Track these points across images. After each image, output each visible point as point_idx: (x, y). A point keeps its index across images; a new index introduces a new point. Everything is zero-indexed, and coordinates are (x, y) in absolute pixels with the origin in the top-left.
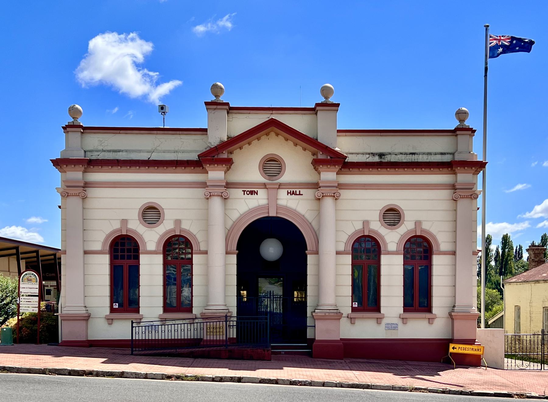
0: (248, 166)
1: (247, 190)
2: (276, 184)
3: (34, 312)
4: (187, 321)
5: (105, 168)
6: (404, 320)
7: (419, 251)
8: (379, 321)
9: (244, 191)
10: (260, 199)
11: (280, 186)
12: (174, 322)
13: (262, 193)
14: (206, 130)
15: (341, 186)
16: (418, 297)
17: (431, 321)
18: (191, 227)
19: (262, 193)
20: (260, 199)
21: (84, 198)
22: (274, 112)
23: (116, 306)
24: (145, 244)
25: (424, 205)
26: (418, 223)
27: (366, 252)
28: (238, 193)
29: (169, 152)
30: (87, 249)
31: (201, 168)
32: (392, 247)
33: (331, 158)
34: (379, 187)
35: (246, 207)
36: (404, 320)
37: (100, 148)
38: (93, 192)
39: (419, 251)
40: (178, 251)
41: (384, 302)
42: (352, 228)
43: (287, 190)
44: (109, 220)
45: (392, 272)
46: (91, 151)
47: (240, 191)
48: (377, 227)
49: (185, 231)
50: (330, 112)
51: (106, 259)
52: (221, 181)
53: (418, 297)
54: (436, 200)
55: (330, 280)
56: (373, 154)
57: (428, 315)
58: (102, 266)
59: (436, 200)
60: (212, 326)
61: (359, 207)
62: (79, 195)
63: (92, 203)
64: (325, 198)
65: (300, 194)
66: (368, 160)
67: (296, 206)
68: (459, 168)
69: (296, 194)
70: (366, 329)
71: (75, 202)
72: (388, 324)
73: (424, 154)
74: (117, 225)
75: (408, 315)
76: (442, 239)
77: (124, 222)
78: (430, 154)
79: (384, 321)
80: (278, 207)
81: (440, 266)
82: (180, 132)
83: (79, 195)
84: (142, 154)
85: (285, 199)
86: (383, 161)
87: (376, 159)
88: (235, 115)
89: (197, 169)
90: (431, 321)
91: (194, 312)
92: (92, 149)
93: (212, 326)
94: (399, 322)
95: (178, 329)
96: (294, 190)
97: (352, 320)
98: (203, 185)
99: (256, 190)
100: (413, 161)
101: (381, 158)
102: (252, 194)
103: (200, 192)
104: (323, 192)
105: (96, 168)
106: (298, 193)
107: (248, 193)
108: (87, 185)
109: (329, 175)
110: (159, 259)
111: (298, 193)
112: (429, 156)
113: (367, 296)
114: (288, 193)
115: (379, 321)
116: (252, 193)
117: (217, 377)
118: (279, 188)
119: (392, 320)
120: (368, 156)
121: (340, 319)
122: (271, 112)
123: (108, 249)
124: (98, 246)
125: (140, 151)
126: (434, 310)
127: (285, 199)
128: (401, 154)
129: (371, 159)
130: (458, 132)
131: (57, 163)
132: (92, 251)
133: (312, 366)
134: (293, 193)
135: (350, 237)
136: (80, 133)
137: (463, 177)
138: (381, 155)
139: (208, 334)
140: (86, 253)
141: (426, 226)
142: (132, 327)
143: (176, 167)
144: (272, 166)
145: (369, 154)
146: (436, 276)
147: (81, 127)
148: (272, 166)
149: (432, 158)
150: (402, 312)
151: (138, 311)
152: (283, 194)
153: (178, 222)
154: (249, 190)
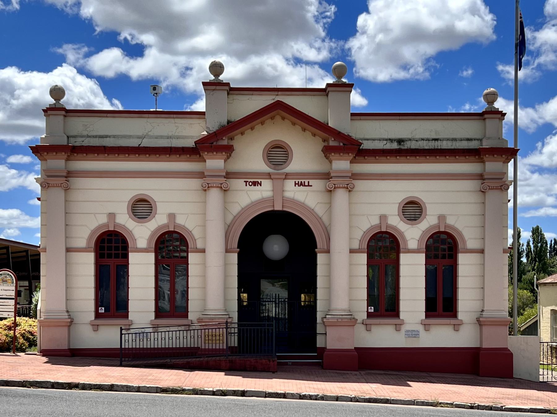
0: (251, 154)
1: (249, 180)
6: (427, 327)
7: (443, 250)
8: (398, 327)
9: (246, 182)
10: (265, 190)
11: (287, 176)
13: (267, 185)
15: (355, 176)
16: (441, 301)
18: (187, 222)
19: (267, 185)
20: (265, 190)
21: (67, 189)
22: (280, 93)
23: (102, 310)
24: (405, 241)
25: (448, 200)
28: (239, 183)
29: (162, 137)
31: (198, 156)
32: (142, 243)
35: (249, 199)
36: (427, 327)
37: (85, 133)
38: (79, 183)
39: (443, 250)
40: (172, 249)
42: (367, 223)
43: (294, 180)
44: (95, 214)
45: (413, 273)
47: (292, 182)
48: (396, 222)
51: (90, 258)
52: (220, 170)
53: (441, 301)
55: (342, 282)
56: (391, 140)
57: (453, 321)
58: (86, 265)
61: (379, 200)
65: (309, 185)
67: (306, 199)
70: (384, 337)
71: (58, 194)
76: (469, 237)
77: (383, 218)
79: (404, 328)
80: (284, 200)
81: (466, 265)
82: (175, 116)
83: (61, 186)
84: (131, 140)
85: (292, 190)
86: (402, 147)
87: (395, 146)
88: (235, 97)
90: (456, 327)
92: (76, 134)
94: (421, 328)
96: (302, 178)
98: (201, 175)
99: (259, 181)
101: (400, 144)
102: (255, 185)
103: (195, 183)
104: (335, 182)
106: (306, 184)
107: (251, 184)
108: (70, 174)
109: (342, 164)
110: (151, 257)
111: (306, 184)
112: (454, 143)
113: (384, 301)
114: (295, 184)
116: (255, 184)
118: (285, 179)
119: (413, 327)
120: (385, 142)
122: (276, 93)
124: (82, 243)
125: (130, 137)
126: (460, 316)
127: (292, 190)
128: (423, 139)
130: (486, 116)
134: (302, 184)
138: (400, 141)
140: (68, 250)
141: (450, 221)
142: (121, 334)
144: (278, 153)
145: (386, 140)
148: (278, 153)
150: (423, 317)
152: (290, 184)
153: (441, 218)
154: (252, 180)
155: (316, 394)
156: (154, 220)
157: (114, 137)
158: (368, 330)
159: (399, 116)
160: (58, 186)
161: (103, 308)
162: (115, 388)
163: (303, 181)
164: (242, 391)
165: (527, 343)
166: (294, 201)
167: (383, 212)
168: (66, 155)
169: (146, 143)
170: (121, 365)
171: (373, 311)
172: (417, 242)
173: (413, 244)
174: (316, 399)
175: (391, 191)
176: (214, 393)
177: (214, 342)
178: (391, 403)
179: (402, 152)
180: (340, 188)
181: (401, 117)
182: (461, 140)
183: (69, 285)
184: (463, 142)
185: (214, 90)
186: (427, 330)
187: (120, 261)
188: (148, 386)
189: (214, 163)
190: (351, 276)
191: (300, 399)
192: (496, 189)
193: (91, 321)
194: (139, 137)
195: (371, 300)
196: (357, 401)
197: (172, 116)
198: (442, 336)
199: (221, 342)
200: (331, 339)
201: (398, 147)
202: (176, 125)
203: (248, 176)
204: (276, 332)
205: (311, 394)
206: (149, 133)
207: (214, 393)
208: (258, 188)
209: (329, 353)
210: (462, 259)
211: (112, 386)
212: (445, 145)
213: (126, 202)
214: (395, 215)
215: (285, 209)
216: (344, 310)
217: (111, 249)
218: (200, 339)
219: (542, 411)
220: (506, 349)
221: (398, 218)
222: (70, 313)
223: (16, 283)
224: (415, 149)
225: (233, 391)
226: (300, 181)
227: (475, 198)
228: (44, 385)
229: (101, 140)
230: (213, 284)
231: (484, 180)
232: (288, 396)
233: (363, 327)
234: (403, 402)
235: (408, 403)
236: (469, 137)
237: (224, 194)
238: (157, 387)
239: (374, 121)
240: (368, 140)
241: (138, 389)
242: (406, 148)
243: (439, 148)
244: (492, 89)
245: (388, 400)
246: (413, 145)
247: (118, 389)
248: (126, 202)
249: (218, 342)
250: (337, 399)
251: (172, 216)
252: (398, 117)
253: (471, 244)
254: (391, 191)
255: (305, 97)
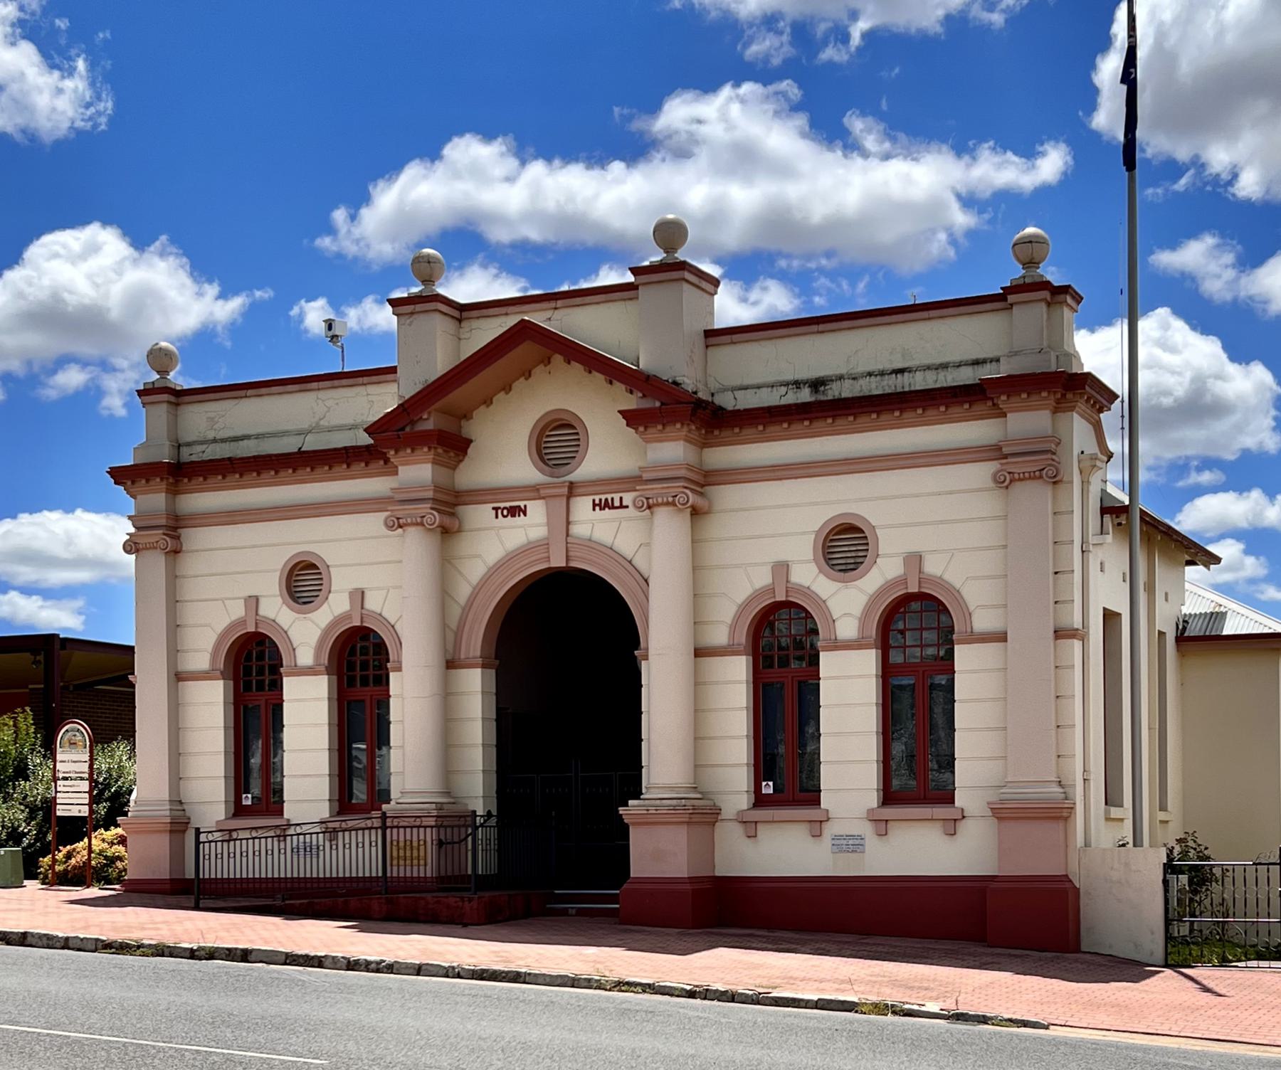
0: (503, 449)
1: (502, 505)
2: (561, 485)
3: (82, 814)
4: (272, 833)
5: (748, 432)
6: (882, 826)
7: (917, 634)
8: (817, 827)
9: (496, 509)
10: (534, 523)
12: (254, 834)
13: (537, 510)
14: (393, 370)
16: (917, 765)
17: (952, 826)
19: (537, 510)
21: (175, 552)
22: (560, 303)
23: (768, 788)
25: (932, 514)
26: (914, 560)
27: (782, 649)
29: (340, 428)
30: (1064, 623)
31: (382, 462)
32: (847, 629)
33: (662, 404)
34: (811, 471)
35: (502, 546)
36: (882, 826)
37: (211, 435)
38: (728, 496)
39: (917, 634)
40: (360, 662)
41: (828, 778)
42: (740, 586)
43: (591, 498)
44: (223, 600)
45: (849, 694)
46: (189, 444)
48: (809, 577)
49: (939, 582)
50: (665, 285)
52: (423, 487)
53: (917, 765)
54: (959, 492)
55: (690, 722)
56: (797, 384)
57: (940, 811)
58: (210, 705)
59: (959, 492)
60: (314, 842)
61: (771, 529)
62: (1041, 477)
63: (192, 564)
64: (1018, 484)
65: (622, 506)
66: (784, 401)
67: (610, 536)
68: (1004, 398)
69: (613, 507)
70: (784, 852)
72: (837, 837)
73: (929, 368)
74: (763, 578)
75: (890, 812)
76: (979, 602)
77: (781, 568)
78: (944, 366)
79: (830, 830)
82: (366, 379)
83: (1041, 477)
84: (286, 440)
85: (588, 521)
86: (822, 398)
87: (805, 395)
88: (475, 324)
89: (980, 408)
90: (952, 826)
91: (957, 803)
92: (195, 438)
93: (314, 842)
94: (867, 830)
95: (357, 856)
97: (750, 827)
98: (995, 452)
99: (522, 504)
100: (899, 390)
101: (817, 391)
102: (513, 516)
103: (981, 473)
104: (648, 494)
105: (726, 433)
106: (617, 503)
108: (705, 480)
110: (868, 661)
111: (617, 503)
112: (942, 374)
113: (786, 763)
114: (594, 505)
115: (817, 827)
116: (514, 512)
117: (484, 971)
119: (850, 828)
120: (783, 389)
121: (714, 824)
122: (553, 304)
123: (743, 640)
125: (285, 433)
127: (588, 521)
128: (870, 374)
129: (792, 398)
130: (1011, 298)
131: (120, 475)
132: (192, 673)
133: (834, 947)
134: (607, 505)
135: (956, 594)
136: (1043, 306)
137: (1027, 421)
138: (817, 384)
139: (395, 862)
141: (932, 567)
143: (879, 413)
144: (557, 440)
145: (787, 384)
146: (961, 701)
147: (1046, 285)
148: (557, 440)
149: (949, 378)
151: (817, 802)
154: (508, 504)
155: (378, 959)
156: (325, 605)
157: (258, 436)
158: (752, 836)
159: (818, 323)
160: (1035, 478)
161: (771, 783)
162: (29, 939)
163: (609, 497)
164: (243, 950)
165: (1127, 865)
166: (590, 544)
167: (782, 557)
168: (685, 428)
169: (312, 443)
170: (197, 908)
171: (771, 791)
172: (857, 622)
173: (847, 629)
174: (378, 971)
175: (784, 506)
176: (192, 954)
177: (408, 862)
178: (524, 982)
179: (822, 408)
180: (658, 505)
181: (822, 327)
182: (959, 365)
183: (180, 748)
184: (963, 369)
185: (412, 313)
186: (883, 834)
187: (372, 689)
188: (82, 936)
189: (417, 472)
190: (699, 711)
191: (348, 969)
192: (1030, 478)
193: (870, 811)
194: (300, 433)
195: (764, 764)
196: (459, 976)
197: (360, 380)
198: (920, 851)
199: (422, 862)
200: (656, 853)
201: (813, 399)
202: (370, 398)
203: (498, 497)
204: (552, 837)
205: (369, 958)
206: (322, 423)
207: (192, 954)
208: (520, 520)
209: (636, 886)
210: (964, 656)
211: (25, 935)
212: (921, 382)
213: (275, 571)
214: (808, 562)
215: (573, 564)
216: (671, 788)
217: (253, 667)
218: (244, 859)
219: (847, 1006)
220: (1066, 878)
221: (813, 568)
222: (185, 807)
223: (91, 746)
224: (853, 399)
225: (228, 949)
226: (603, 497)
227: (989, 504)
228: (803, 1004)
229: (226, 446)
230: (440, 735)
231: (1005, 457)
232: (327, 963)
233: (737, 831)
234: (548, 980)
235: (559, 981)
236: (974, 357)
237: (443, 541)
238: (97, 940)
239: (786, 341)
240: (746, 388)
241: (66, 944)
242: (830, 397)
243: (907, 389)
244: (1031, 230)
245: (518, 974)
246: (847, 390)
247: (34, 941)
248: (275, 571)
249: (402, 862)
250: (419, 970)
251: (359, 596)
252: (814, 328)
253: (983, 621)
254: (784, 506)
255: (610, 304)
